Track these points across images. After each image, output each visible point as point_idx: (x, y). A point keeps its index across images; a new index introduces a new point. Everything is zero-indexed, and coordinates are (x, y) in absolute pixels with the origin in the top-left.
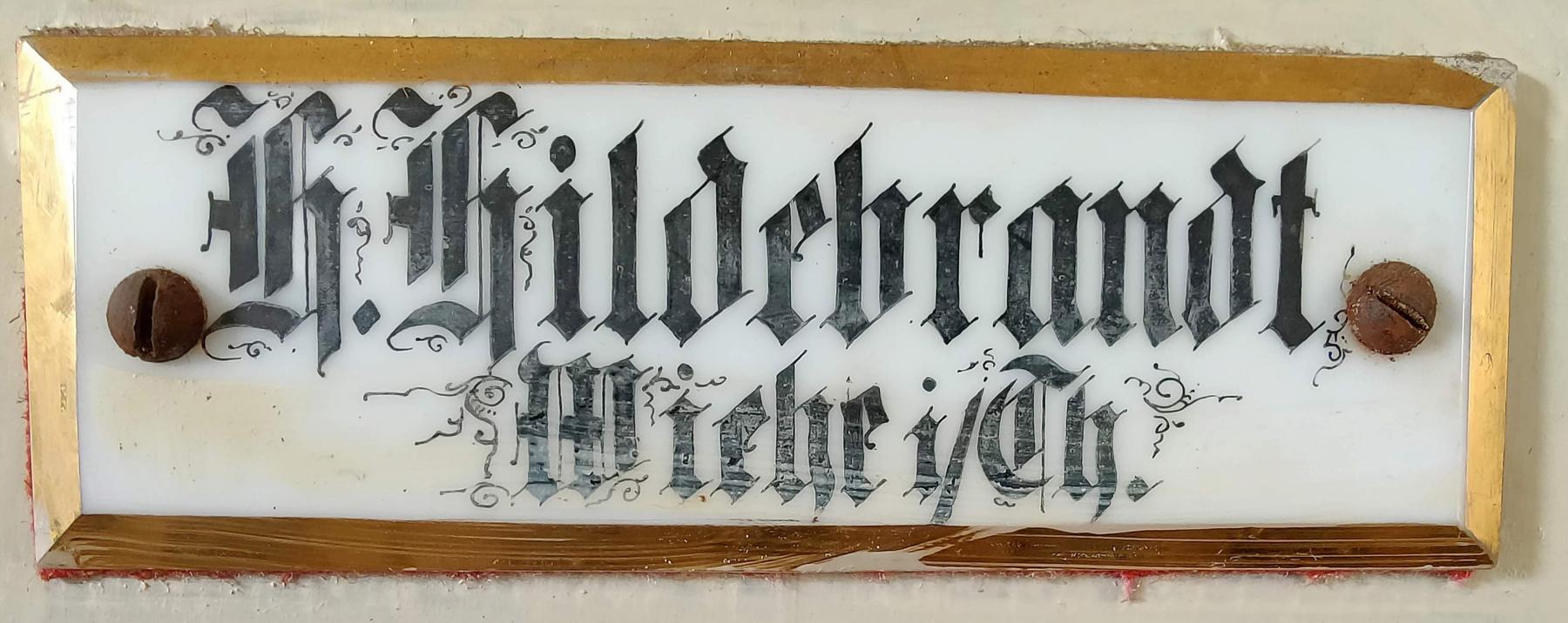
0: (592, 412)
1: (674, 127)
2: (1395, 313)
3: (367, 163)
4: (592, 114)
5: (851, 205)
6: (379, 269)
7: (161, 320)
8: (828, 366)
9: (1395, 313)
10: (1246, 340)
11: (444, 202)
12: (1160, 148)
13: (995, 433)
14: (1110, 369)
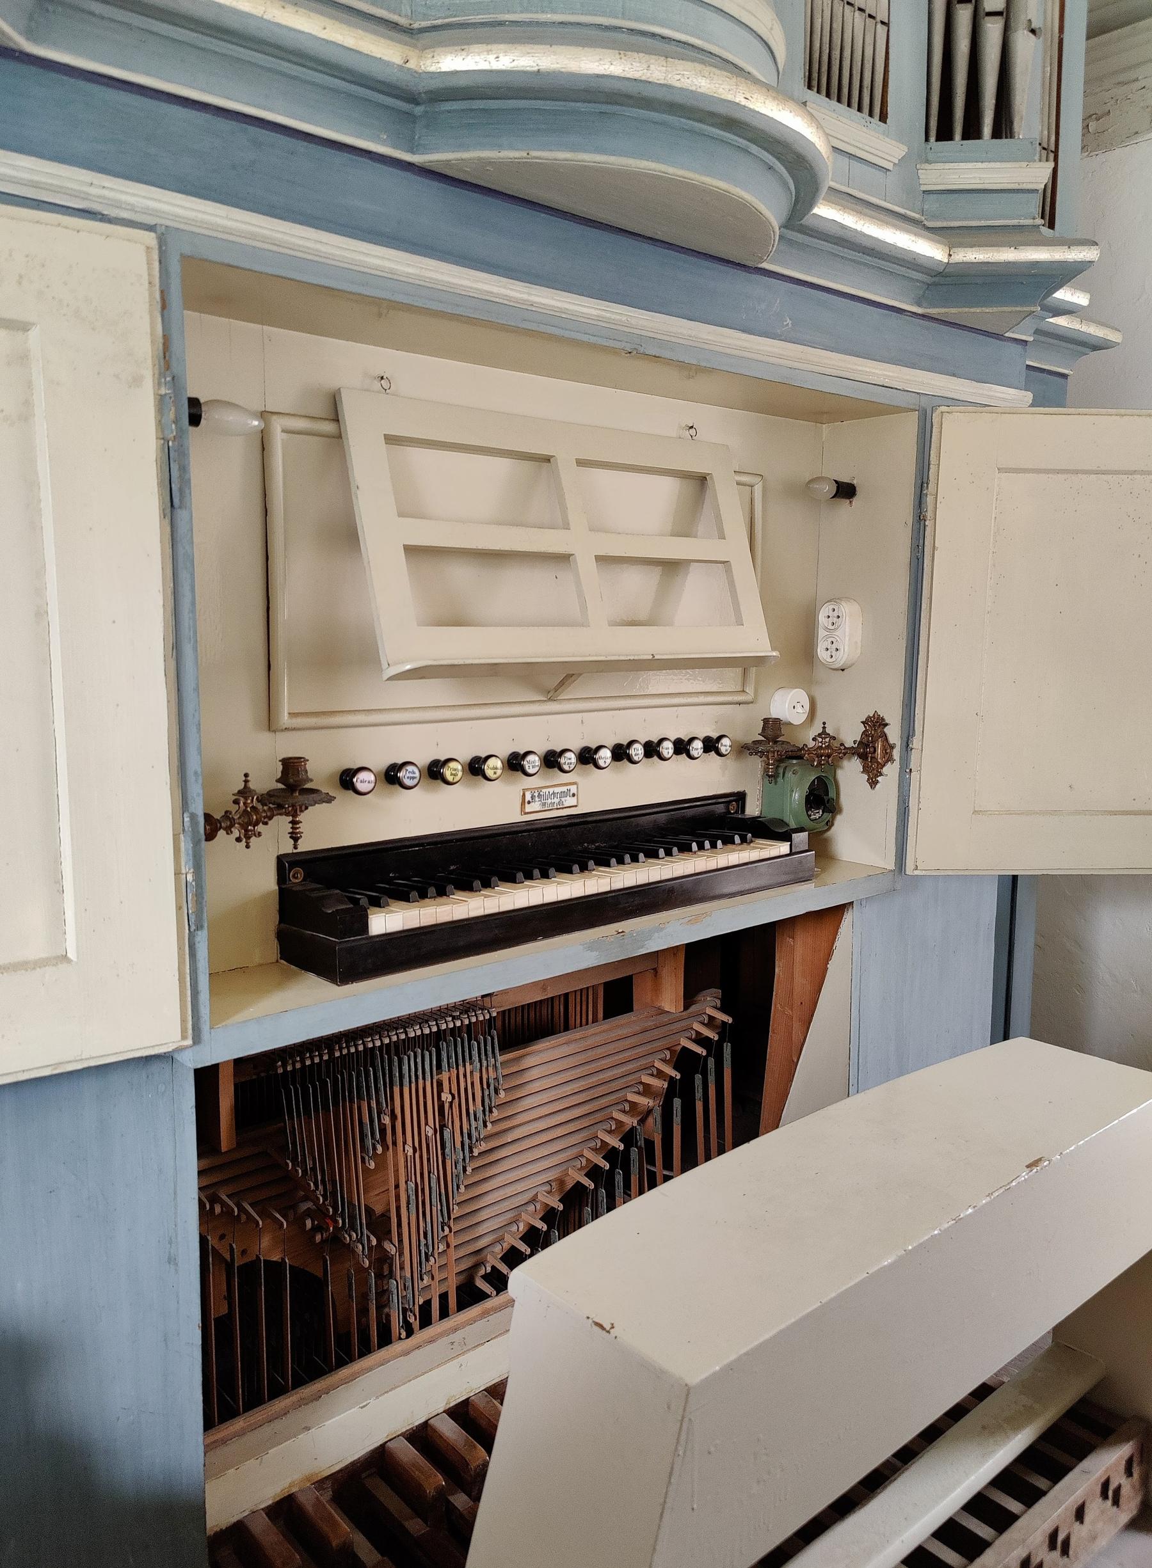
7: (529, 802)
11: (539, 795)
12: (564, 789)
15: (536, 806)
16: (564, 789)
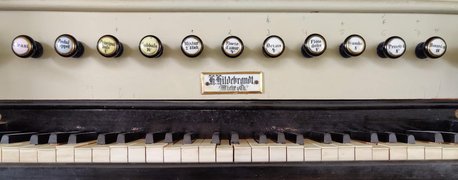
0: (224, 87)
1: (227, 76)
2: (257, 82)
3: (215, 78)
4: (224, 76)
5: (234, 79)
6: (216, 82)
7: (207, 84)
8: (233, 85)
9: (257, 82)
10: (251, 84)
11: (218, 79)
12: (247, 76)
13: (240, 88)
14: (245, 85)
15: (215, 88)
16: (247, 76)
